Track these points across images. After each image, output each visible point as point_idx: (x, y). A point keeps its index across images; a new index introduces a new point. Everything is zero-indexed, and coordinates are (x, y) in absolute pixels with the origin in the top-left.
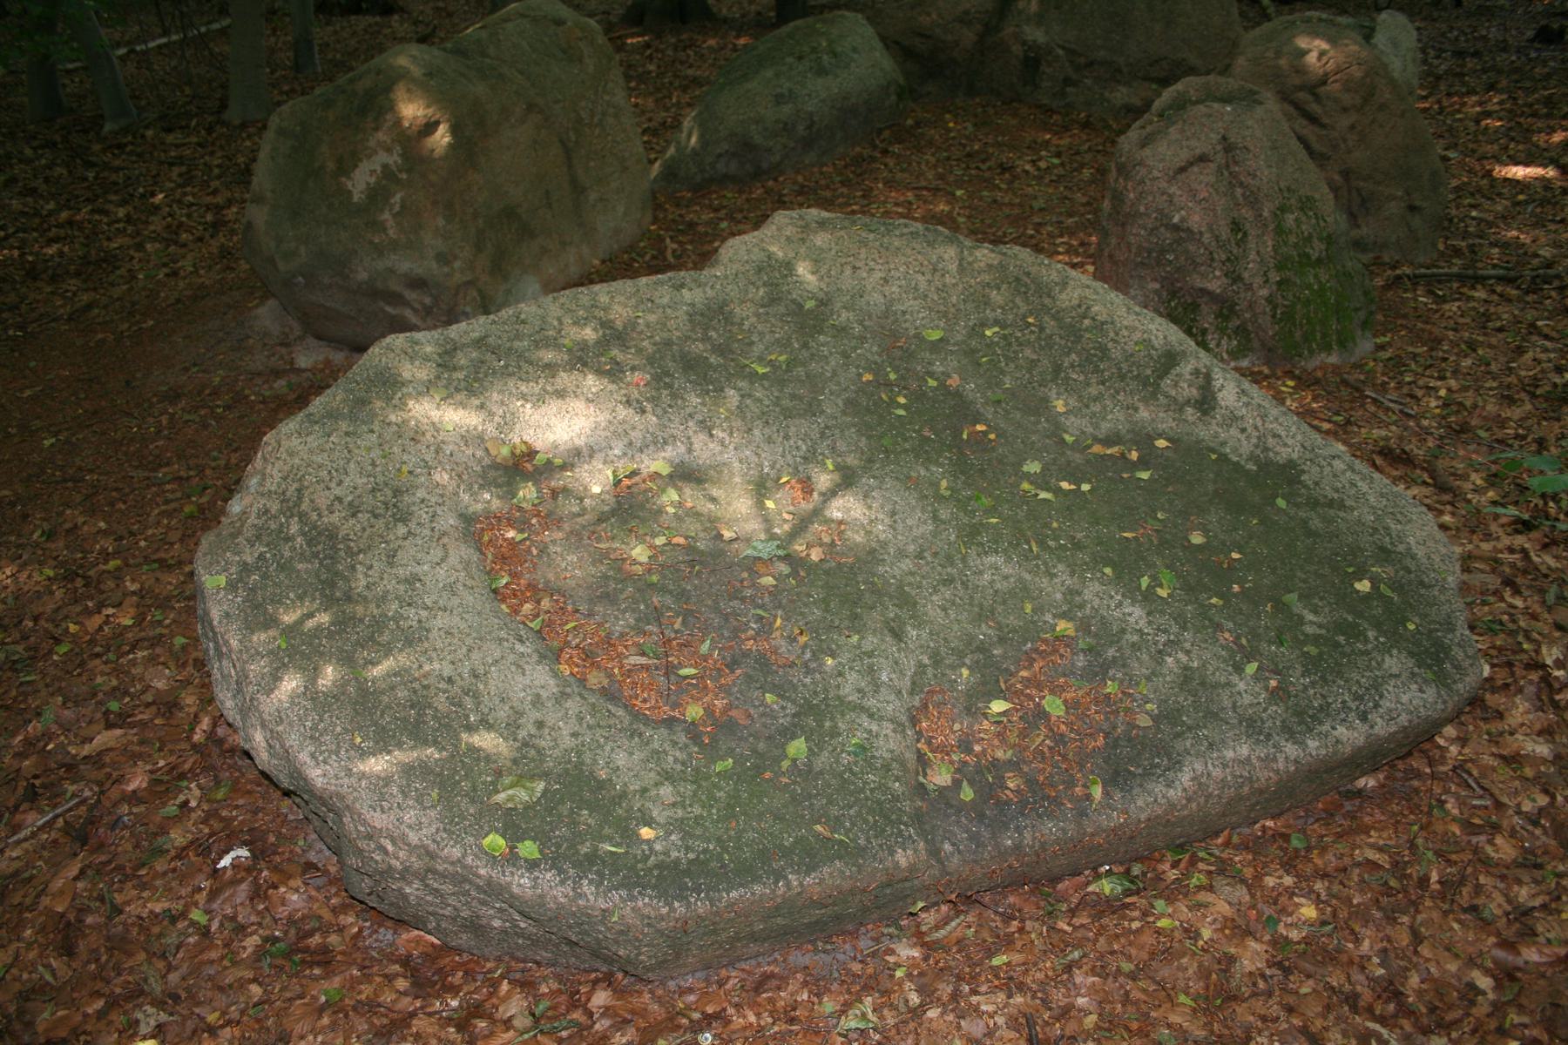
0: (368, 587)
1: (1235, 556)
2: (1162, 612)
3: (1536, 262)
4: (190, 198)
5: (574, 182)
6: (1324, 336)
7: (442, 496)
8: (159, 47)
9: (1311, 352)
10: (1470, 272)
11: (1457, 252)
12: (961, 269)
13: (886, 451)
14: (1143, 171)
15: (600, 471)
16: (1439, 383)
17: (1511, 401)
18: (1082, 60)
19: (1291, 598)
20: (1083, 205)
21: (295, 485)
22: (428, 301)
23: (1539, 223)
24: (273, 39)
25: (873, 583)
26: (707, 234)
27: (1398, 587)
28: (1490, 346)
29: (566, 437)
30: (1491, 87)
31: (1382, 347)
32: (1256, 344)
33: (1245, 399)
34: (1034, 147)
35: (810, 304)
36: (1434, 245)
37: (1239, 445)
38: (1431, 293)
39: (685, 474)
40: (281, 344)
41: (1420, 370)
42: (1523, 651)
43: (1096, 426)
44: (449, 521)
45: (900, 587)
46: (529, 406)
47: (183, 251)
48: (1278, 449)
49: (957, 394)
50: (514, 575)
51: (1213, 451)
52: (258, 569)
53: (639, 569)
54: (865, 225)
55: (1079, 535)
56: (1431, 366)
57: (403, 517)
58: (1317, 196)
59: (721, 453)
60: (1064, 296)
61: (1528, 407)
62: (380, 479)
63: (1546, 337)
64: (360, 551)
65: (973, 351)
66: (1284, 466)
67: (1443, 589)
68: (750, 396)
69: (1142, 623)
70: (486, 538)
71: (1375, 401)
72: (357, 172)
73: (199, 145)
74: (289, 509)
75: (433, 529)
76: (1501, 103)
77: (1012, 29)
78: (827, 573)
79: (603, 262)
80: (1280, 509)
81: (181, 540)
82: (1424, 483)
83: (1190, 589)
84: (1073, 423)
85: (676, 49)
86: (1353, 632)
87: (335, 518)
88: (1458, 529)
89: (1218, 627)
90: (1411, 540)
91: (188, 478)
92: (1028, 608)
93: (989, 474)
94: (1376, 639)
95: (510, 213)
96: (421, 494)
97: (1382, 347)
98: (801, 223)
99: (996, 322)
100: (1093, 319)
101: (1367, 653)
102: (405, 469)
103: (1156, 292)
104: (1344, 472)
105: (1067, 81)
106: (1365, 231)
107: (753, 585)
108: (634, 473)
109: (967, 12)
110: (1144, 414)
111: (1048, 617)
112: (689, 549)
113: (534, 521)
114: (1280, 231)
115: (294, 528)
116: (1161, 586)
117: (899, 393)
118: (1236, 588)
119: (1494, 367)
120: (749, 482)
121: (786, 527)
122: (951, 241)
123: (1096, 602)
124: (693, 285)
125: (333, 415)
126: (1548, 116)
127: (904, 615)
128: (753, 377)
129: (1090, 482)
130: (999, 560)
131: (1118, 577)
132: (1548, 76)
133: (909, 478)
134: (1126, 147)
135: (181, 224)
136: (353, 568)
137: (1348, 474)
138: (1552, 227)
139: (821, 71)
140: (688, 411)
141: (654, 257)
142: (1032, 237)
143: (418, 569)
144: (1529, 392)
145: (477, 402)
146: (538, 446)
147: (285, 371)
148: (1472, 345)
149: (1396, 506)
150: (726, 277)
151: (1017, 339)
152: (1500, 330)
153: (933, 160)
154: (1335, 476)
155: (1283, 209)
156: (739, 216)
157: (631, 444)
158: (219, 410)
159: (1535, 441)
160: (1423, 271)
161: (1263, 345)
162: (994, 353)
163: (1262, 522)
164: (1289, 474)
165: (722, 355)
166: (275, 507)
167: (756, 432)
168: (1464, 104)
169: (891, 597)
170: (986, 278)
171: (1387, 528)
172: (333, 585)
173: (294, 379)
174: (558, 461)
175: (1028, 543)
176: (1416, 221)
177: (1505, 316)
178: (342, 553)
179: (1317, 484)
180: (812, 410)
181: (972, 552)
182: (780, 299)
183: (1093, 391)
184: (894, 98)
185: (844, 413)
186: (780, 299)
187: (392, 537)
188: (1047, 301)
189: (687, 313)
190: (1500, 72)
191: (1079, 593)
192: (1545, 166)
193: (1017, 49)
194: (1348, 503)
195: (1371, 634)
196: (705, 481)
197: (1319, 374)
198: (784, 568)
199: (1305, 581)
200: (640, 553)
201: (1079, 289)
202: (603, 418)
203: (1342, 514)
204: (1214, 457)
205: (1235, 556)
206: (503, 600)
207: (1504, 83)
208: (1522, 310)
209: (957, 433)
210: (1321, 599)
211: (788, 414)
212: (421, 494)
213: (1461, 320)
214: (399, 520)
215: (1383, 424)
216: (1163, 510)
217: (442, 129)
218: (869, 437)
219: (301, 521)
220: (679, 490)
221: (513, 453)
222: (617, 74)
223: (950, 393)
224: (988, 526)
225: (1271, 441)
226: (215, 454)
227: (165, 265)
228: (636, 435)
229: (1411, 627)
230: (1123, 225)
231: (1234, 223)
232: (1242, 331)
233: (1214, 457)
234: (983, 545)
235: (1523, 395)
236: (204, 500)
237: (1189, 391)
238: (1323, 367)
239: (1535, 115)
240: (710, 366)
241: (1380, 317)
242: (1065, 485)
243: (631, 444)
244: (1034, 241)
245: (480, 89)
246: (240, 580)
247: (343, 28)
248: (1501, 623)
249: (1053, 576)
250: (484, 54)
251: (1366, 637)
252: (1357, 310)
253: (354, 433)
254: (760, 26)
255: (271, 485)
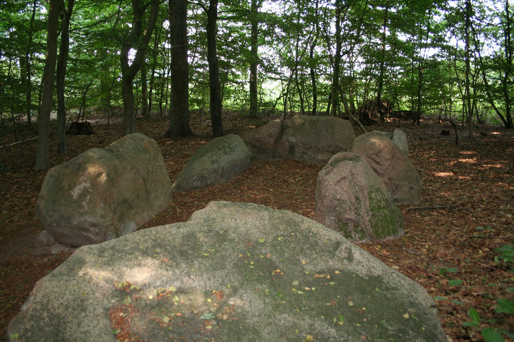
0: (70, 336)
1: (364, 309)
2: (341, 330)
3: (450, 202)
4: (20, 195)
5: (147, 190)
6: (388, 231)
7: (98, 302)
8: (14, 145)
9: (385, 236)
10: (431, 207)
11: (427, 200)
12: (270, 219)
13: (247, 281)
14: (327, 183)
15: (152, 291)
16: (425, 244)
17: (448, 248)
18: (308, 147)
19: (383, 322)
20: (310, 192)
21: (47, 299)
22: (97, 231)
23: (450, 190)
24: (52, 142)
25: (244, 326)
26: (190, 206)
27: (418, 315)
28: (440, 230)
29: (141, 279)
30: (431, 149)
31: (406, 233)
32: (367, 235)
33: (362, 256)
34: (294, 174)
35: (221, 232)
36: (419, 199)
37: (362, 271)
38: (420, 214)
39: (180, 291)
40: (47, 246)
41: (419, 240)
42: (462, 333)
43: (316, 268)
44: (100, 310)
45: (254, 327)
46: (128, 269)
47: (15, 213)
48: (374, 271)
49: (270, 260)
50: (122, 329)
51: (354, 273)
52: (31, 330)
53: (166, 325)
54: (239, 206)
55: (312, 305)
56: (422, 238)
57: (84, 310)
58: (381, 187)
59: (193, 283)
60: (302, 226)
61: (454, 249)
62: (77, 296)
63: (456, 226)
64: (68, 322)
65: (275, 245)
66: (377, 277)
67: (432, 315)
68: (202, 263)
69: (335, 334)
70: (113, 316)
71: (406, 251)
72: (75, 189)
73: (24, 177)
74: (44, 308)
75: (94, 314)
76: (434, 154)
77: (285, 138)
78: (229, 323)
79: (156, 216)
80: (377, 292)
81: (4, 317)
82: (424, 277)
83: (350, 321)
84: (308, 267)
85: (181, 145)
86: (405, 333)
87: (60, 311)
88: (436, 292)
89: (360, 334)
90: (420, 299)
91: (10, 294)
92: (297, 331)
93: (282, 286)
94: (412, 334)
95: (125, 201)
96: (91, 301)
97: (406, 233)
98: (218, 205)
99: (282, 235)
100: (313, 233)
101: (410, 339)
102: (85, 292)
103: (334, 220)
104: (396, 278)
105: (303, 153)
106: (398, 196)
107: (204, 329)
108: (164, 291)
109: (271, 133)
110: (331, 263)
111: (304, 334)
112: (183, 317)
113: (130, 309)
114: (370, 199)
115: (45, 315)
116: (340, 321)
117: (251, 261)
118: (365, 320)
119: (442, 237)
120: (202, 293)
121: (215, 308)
122: (266, 209)
123: (319, 328)
124: (183, 227)
125: (61, 274)
126: (448, 157)
127: (255, 336)
128: (203, 257)
129: (315, 287)
130: (286, 315)
131: (326, 319)
132: (446, 145)
133: (255, 289)
134: (321, 175)
135: (16, 204)
136: (65, 329)
137: (398, 278)
138: (454, 191)
139: (226, 153)
140: (182, 269)
141: (173, 214)
142: (295, 203)
143: (88, 329)
144: (453, 244)
145: (111, 269)
146: (132, 282)
147: (47, 255)
148: (435, 231)
149: (414, 287)
150: (194, 224)
151: (289, 240)
152: (442, 225)
153: (262, 179)
154: (393, 279)
155: (371, 192)
156: (201, 200)
157: (163, 281)
158: (23, 269)
159: (457, 260)
160: (417, 207)
161: (369, 235)
162: (282, 245)
163: (372, 296)
164: (378, 280)
165: (193, 250)
166: (39, 307)
167: (204, 276)
168: (424, 154)
169: (251, 331)
170: (278, 221)
171: (412, 295)
172: (57, 335)
173: (51, 258)
174: (138, 288)
175: (296, 309)
176: (413, 192)
177: (443, 220)
178: (62, 323)
179: (388, 282)
180: (223, 268)
181: (277, 313)
182: (212, 231)
183: (314, 256)
184: (249, 160)
185: (233, 268)
186: (212, 231)
187: (80, 317)
188: (297, 228)
189: (181, 236)
190: (433, 144)
191: (313, 325)
192: (449, 172)
193: (287, 144)
194: (399, 288)
195: (411, 332)
196: (188, 293)
197: (388, 243)
198: (215, 323)
199: (387, 316)
200: (166, 319)
201: (307, 223)
202: (153, 273)
203: (397, 292)
204: (354, 275)
205: (364, 309)
206: (118, 338)
207: (434, 148)
208: (448, 218)
209: (271, 273)
210: (393, 321)
211: (215, 269)
212: (91, 301)
213: (430, 222)
214: (83, 311)
215: (409, 258)
216: (339, 295)
217: (104, 175)
218: (242, 276)
219: (48, 312)
220: (179, 297)
221: (123, 286)
222: (161, 156)
223: (268, 259)
224: (282, 304)
225: (372, 269)
226: (20, 285)
227: (8, 218)
228: (164, 279)
229: (423, 329)
230: (322, 199)
231: (356, 197)
232: (362, 231)
233: (354, 275)
234: (280, 311)
235: (452, 246)
236: (15, 302)
237: (344, 255)
238: (389, 241)
239: (444, 157)
240: (189, 254)
241: (405, 223)
242: (306, 288)
243: (163, 281)
244: (295, 205)
245: (116, 162)
246: (24, 335)
247: (75, 139)
248: (454, 324)
249: (304, 320)
250: (118, 151)
251: (409, 333)
252: (397, 222)
253: (69, 280)
254: (208, 137)
255: (38, 299)
